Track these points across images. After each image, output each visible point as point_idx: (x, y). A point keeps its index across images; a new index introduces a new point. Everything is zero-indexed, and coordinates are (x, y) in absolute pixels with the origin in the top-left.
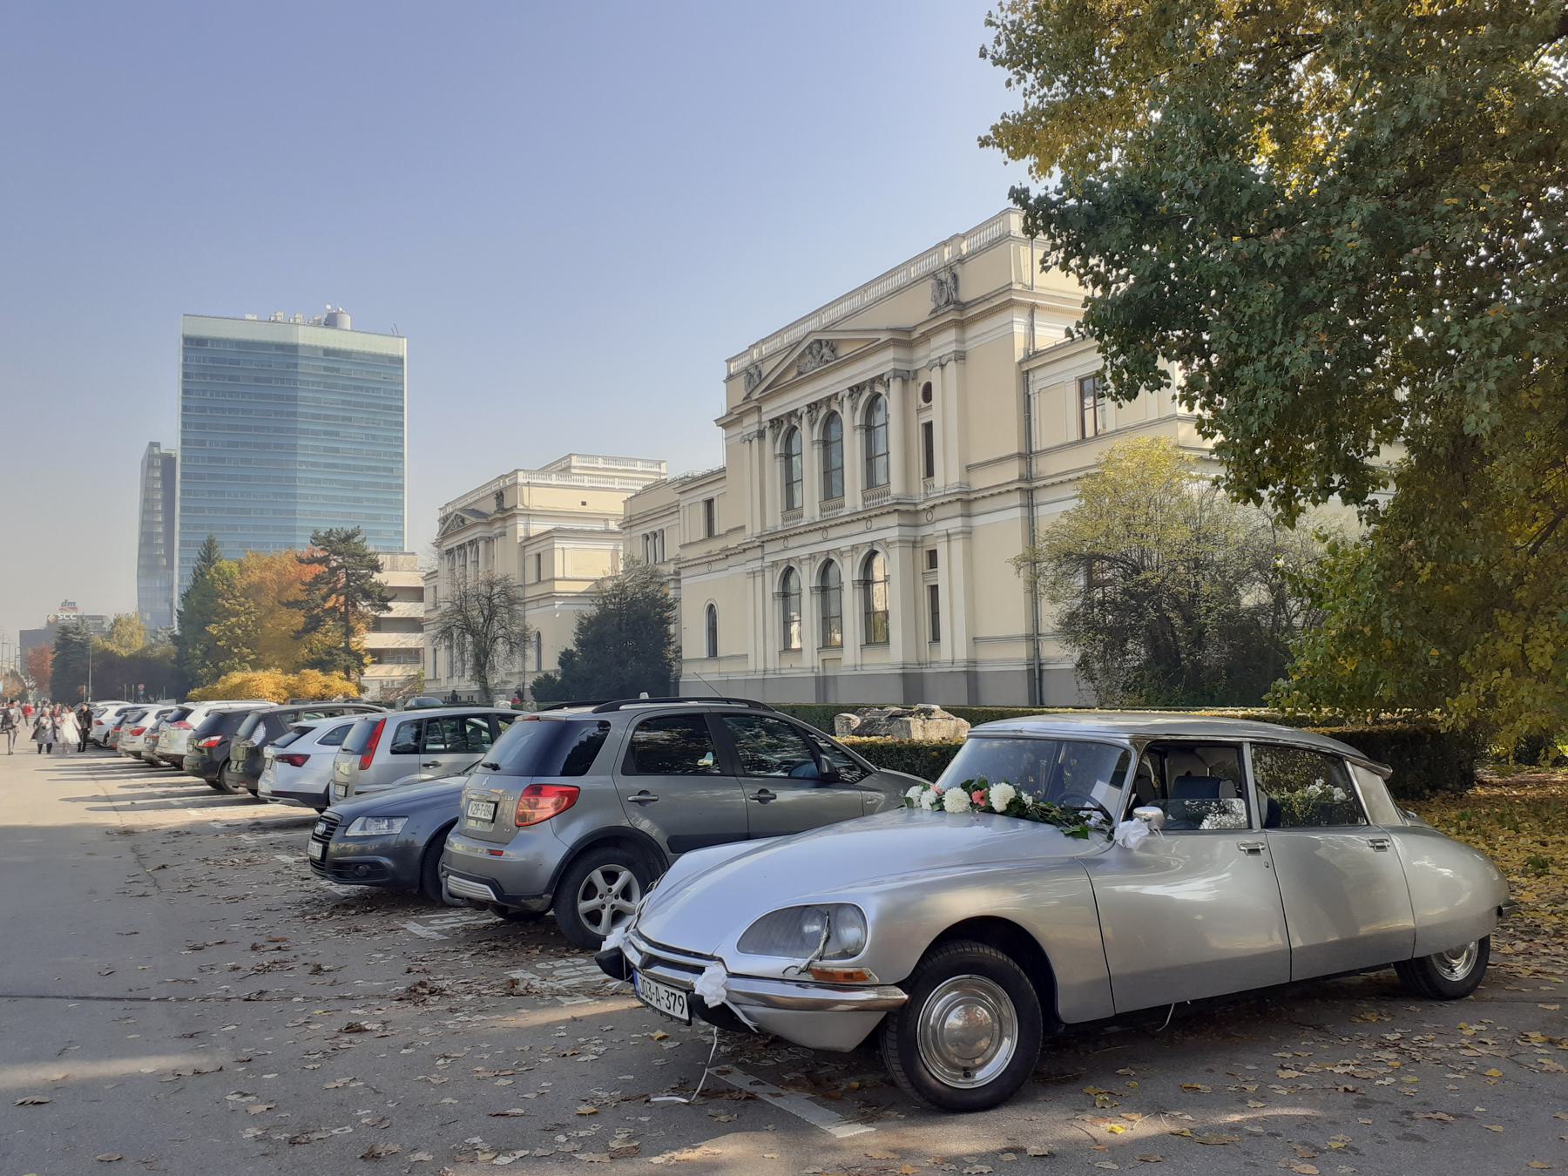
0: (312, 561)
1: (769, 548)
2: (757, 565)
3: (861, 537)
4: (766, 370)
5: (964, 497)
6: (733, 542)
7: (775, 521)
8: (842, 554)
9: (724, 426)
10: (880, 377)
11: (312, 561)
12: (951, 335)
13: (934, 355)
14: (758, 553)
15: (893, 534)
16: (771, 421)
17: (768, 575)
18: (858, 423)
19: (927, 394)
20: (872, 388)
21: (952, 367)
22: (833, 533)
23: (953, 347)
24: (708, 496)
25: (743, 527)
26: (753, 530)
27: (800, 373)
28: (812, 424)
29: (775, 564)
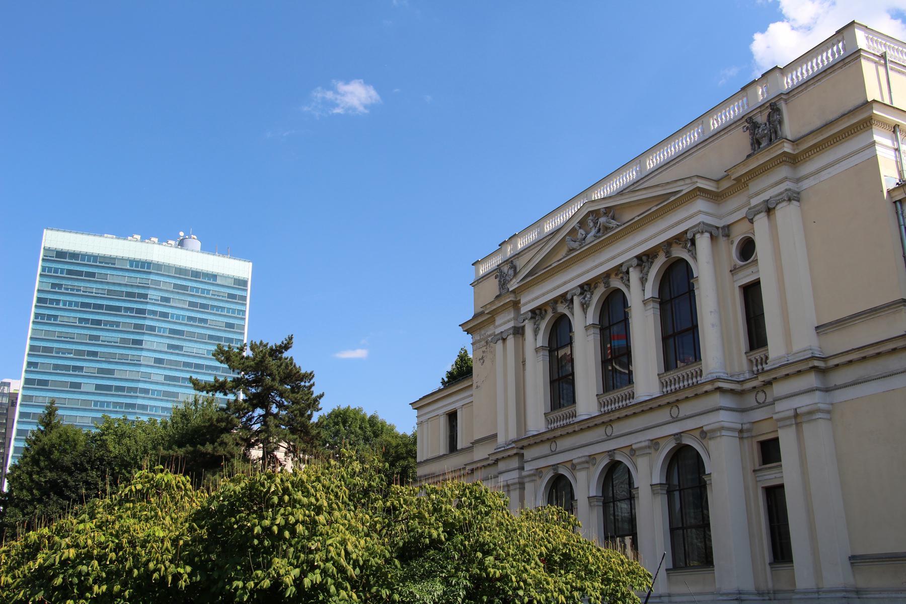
0: (220, 387)
1: (528, 454)
2: (513, 476)
3: (665, 429)
4: (520, 263)
5: (821, 364)
6: (481, 453)
7: (536, 423)
8: (574, 467)
9: (468, 331)
10: (563, 297)
11: (220, 387)
12: (784, 171)
13: (498, 331)
14: (515, 463)
15: (724, 418)
16: (533, 311)
17: (529, 487)
18: (649, 294)
19: (747, 249)
20: (607, 284)
21: (511, 341)
22: (686, 409)
23: (511, 324)
24: (450, 408)
25: (495, 436)
26: (507, 433)
27: (572, 250)
28: (585, 307)
29: (539, 472)
